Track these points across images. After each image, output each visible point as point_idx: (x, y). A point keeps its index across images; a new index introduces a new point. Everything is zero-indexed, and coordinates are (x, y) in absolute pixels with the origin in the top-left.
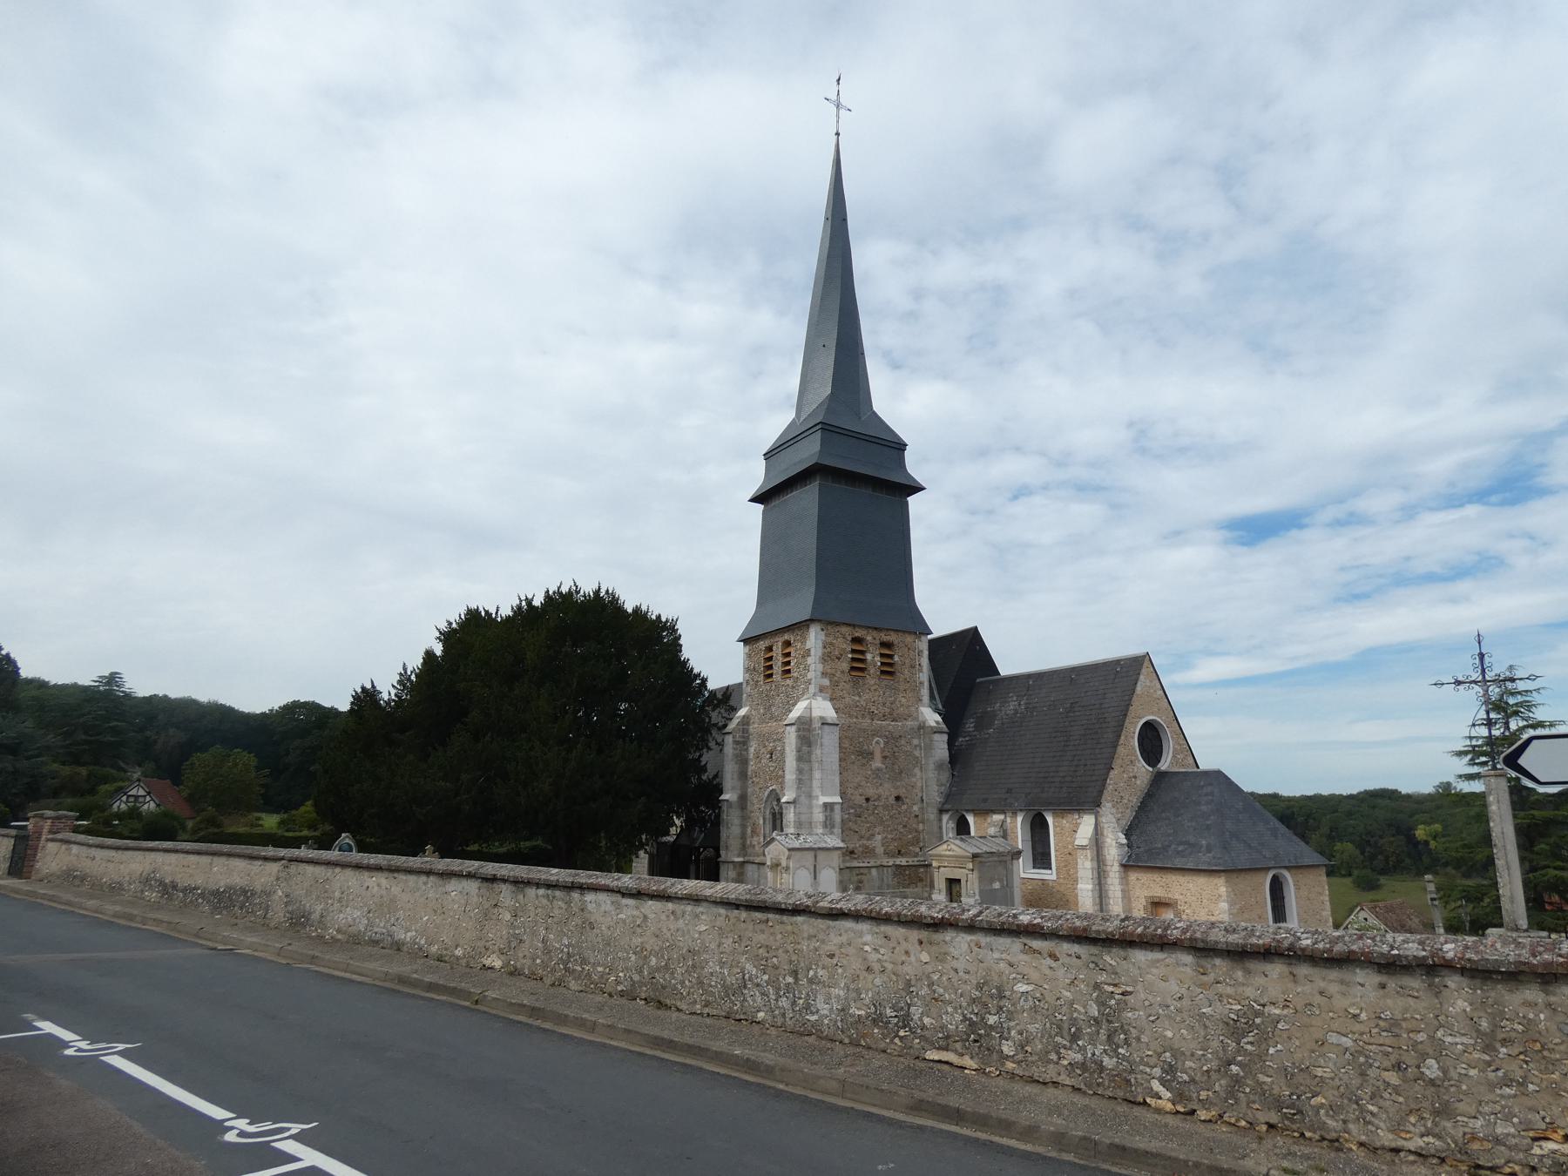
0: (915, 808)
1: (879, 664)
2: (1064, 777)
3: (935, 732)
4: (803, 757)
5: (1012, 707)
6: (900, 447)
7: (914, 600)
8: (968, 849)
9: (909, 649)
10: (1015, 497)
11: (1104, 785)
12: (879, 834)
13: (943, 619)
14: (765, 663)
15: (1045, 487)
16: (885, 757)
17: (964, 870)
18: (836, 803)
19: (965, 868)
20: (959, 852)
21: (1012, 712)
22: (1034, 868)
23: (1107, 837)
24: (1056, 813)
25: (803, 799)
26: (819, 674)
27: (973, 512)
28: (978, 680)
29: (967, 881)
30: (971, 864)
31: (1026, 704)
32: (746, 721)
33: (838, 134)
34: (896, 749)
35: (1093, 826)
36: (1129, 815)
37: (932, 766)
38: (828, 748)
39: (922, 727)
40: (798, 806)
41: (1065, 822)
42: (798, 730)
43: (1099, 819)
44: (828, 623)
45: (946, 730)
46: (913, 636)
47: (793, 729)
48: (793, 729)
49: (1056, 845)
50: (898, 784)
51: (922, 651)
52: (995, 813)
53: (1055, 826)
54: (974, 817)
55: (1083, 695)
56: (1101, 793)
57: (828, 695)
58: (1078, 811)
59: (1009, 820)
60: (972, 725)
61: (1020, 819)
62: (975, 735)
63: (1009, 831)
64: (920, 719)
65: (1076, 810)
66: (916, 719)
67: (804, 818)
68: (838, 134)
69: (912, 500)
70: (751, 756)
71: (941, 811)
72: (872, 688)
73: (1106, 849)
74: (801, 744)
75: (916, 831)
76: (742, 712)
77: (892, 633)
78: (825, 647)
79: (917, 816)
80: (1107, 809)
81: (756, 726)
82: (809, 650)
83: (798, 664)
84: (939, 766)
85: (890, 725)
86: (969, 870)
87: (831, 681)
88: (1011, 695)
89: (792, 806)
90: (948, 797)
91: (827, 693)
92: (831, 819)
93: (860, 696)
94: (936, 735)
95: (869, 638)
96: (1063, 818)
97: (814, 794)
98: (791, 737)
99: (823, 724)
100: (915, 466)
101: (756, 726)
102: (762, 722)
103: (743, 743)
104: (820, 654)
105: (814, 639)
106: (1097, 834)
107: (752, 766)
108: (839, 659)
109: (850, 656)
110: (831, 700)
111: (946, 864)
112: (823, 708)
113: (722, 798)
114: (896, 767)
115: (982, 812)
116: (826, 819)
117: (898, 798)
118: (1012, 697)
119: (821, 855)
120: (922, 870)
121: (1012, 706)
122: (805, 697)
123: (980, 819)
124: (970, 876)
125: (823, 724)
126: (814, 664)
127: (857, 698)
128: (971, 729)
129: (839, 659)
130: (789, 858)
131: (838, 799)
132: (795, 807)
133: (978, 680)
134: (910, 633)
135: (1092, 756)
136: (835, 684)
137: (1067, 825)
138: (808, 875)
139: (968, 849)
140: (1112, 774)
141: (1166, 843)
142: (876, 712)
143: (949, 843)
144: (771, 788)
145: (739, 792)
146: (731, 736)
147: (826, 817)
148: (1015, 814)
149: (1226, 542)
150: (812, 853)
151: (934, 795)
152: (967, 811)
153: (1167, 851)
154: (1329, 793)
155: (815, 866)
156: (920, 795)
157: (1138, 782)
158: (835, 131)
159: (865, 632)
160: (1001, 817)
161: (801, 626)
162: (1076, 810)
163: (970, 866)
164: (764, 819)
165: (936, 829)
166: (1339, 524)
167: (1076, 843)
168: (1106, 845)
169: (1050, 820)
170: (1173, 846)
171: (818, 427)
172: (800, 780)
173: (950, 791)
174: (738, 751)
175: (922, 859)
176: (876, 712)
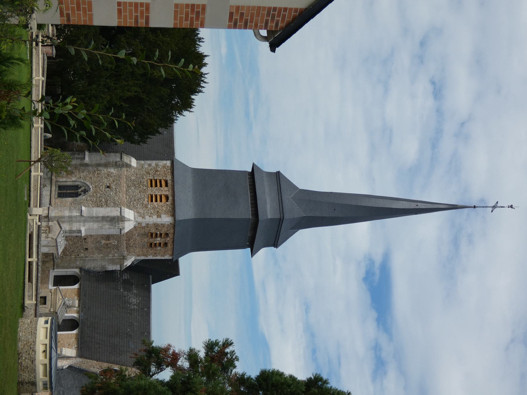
0: (82, 255)
1: (155, 242)
2: (94, 338)
3: (121, 266)
4: (104, 219)
5: (133, 300)
6: (276, 245)
7: (192, 252)
8: (59, 311)
9: (165, 252)
10: (433, 83)
11: (89, 359)
12: (68, 243)
13: (184, 261)
14: (159, 179)
15: (439, 112)
16: (107, 245)
17: (50, 306)
18: (82, 234)
19: (51, 307)
20: (58, 305)
21: (131, 301)
22: (54, 276)
23: (66, 361)
24: (77, 335)
25: (83, 219)
26: (148, 223)
27: (423, 44)
28: (151, 276)
29: (45, 308)
30: (53, 311)
31: (134, 309)
32: (128, 166)
33: (475, 207)
34: (111, 248)
35: (71, 356)
36: (77, 366)
37: (104, 263)
38: (107, 229)
39: (124, 258)
40: (80, 217)
41: (74, 340)
42: (118, 217)
43: (74, 358)
44: (174, 225)
45: (122, 269)
46: (171, 254)
47: (119, 214)
48: (119, 214)
49: (63, 334)
50: (94, 249)
51: (164, 257)
52: (79, 301)
53: (72, 334)
54: (78, 288)
55: (135, 341)
56: (85, 358)
57: (137, 226)
58: (78, 347)
59: (75, 309)
60: (126, 278)
61: (75, 315)
62: (120, 281)
63: (70, 309)
64: (128, 257)
65: (78, 347)
66: (128, 255)
67: (74, 219)
68: (475, 207)
69: (249, 249)
70: (109, 170)
71: (81, 269)
72: (142, 240)
73: (61, 361)
74: (111, 218)
75: (71, 255)
76: (134, 162)
77: (172, 246)
78: (161, 224)
79: (78, 255)
80: (79, 360)
81: (125, 172)
82: (160, 217)
83: (154, 208)
84: (103, 267)
85: (124, 246)
86: (50, 309)
87: (144, 226)
88: (140, 298)
89: (79, 215)
90: (88, 272)
91: (138, 225)
92: (73, 232)
93: (138, 236)
94: (120, 266)
95: (168, 239)
96: (75, 339)
97: (86, 224)
98: (114, 212)
99: (121, 229)
100: (263, 253)
101: (125, 172)
102: (127, 178)
103: (116, 165)
104: (158, 223)
105: (166, 219)
106: (67, 357)
107: (104, 171)
108: (156, 229)
109: (158, 233)
110: (135, 227)
111: (53, 297)
112: (128, 226)
113: (87, 153)
114: (103, 248)
115: (80, 294)
116: (73, 231)
117: (87, 249)
118: (139, 299)
119: (55, 248)
120: (51, 257)
121: (134, 301)
122: (136, 214)
123: (76, 291)
124: (47, 309)
125: (121, 229)
126: (154, 219)
127: (136, 235)
128: (124, 277)
129: (156, 229)
130: (52, 238)
131: (83, 235)
132: (79, 216)
133: (151, 276)
134: (173, 253)
135: (103, 351)
136: (143, 228)
137: (72, 341)
138: (46, 244)
139: (59, 311)
140: (95, 362)
141: (64, 385)
142: (130, 242)
143: (62, 299)
144: (91, 187)
145: (89, 163)
146: (120, 160)
147: (75, 231)
148: (78, 312)
149: (371, 262)
150: (55, 245)
151: (90, 265)
152: (80, 285)
153: (60, 387)
154: (273, 53)
155: (50, 246)
156: (89, 256)
157: (92, 368)
158: (476, 205)
159: (171, 237)
160: (77, 305)
161: (173, 215)
162: (78, 347)
163: (52, 310)
164: (75, 181)
165: (72, 265)
166: (376, 348)
167: (63, 348)
168: (63, 361)
169: (75, 332)
170: (62, 389)
171: (282, 216)
172: (93, 217)
173: (91, 272)
174: (111, 163)
175: (57, 258)
176: (130, 242)
